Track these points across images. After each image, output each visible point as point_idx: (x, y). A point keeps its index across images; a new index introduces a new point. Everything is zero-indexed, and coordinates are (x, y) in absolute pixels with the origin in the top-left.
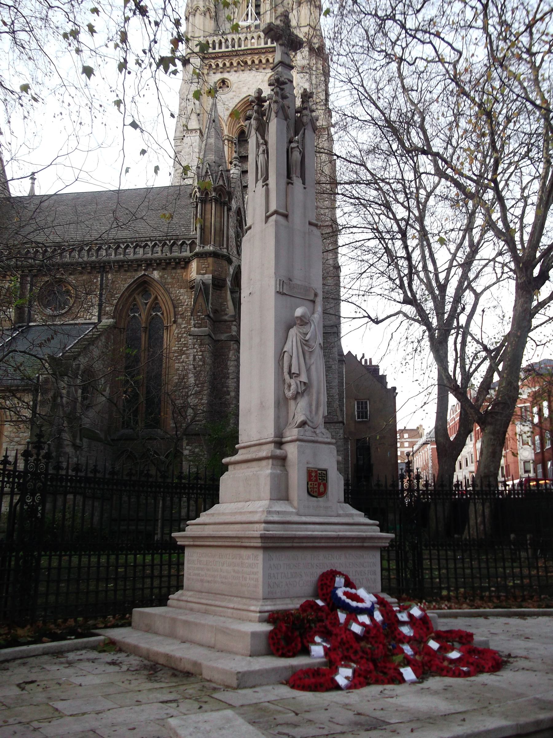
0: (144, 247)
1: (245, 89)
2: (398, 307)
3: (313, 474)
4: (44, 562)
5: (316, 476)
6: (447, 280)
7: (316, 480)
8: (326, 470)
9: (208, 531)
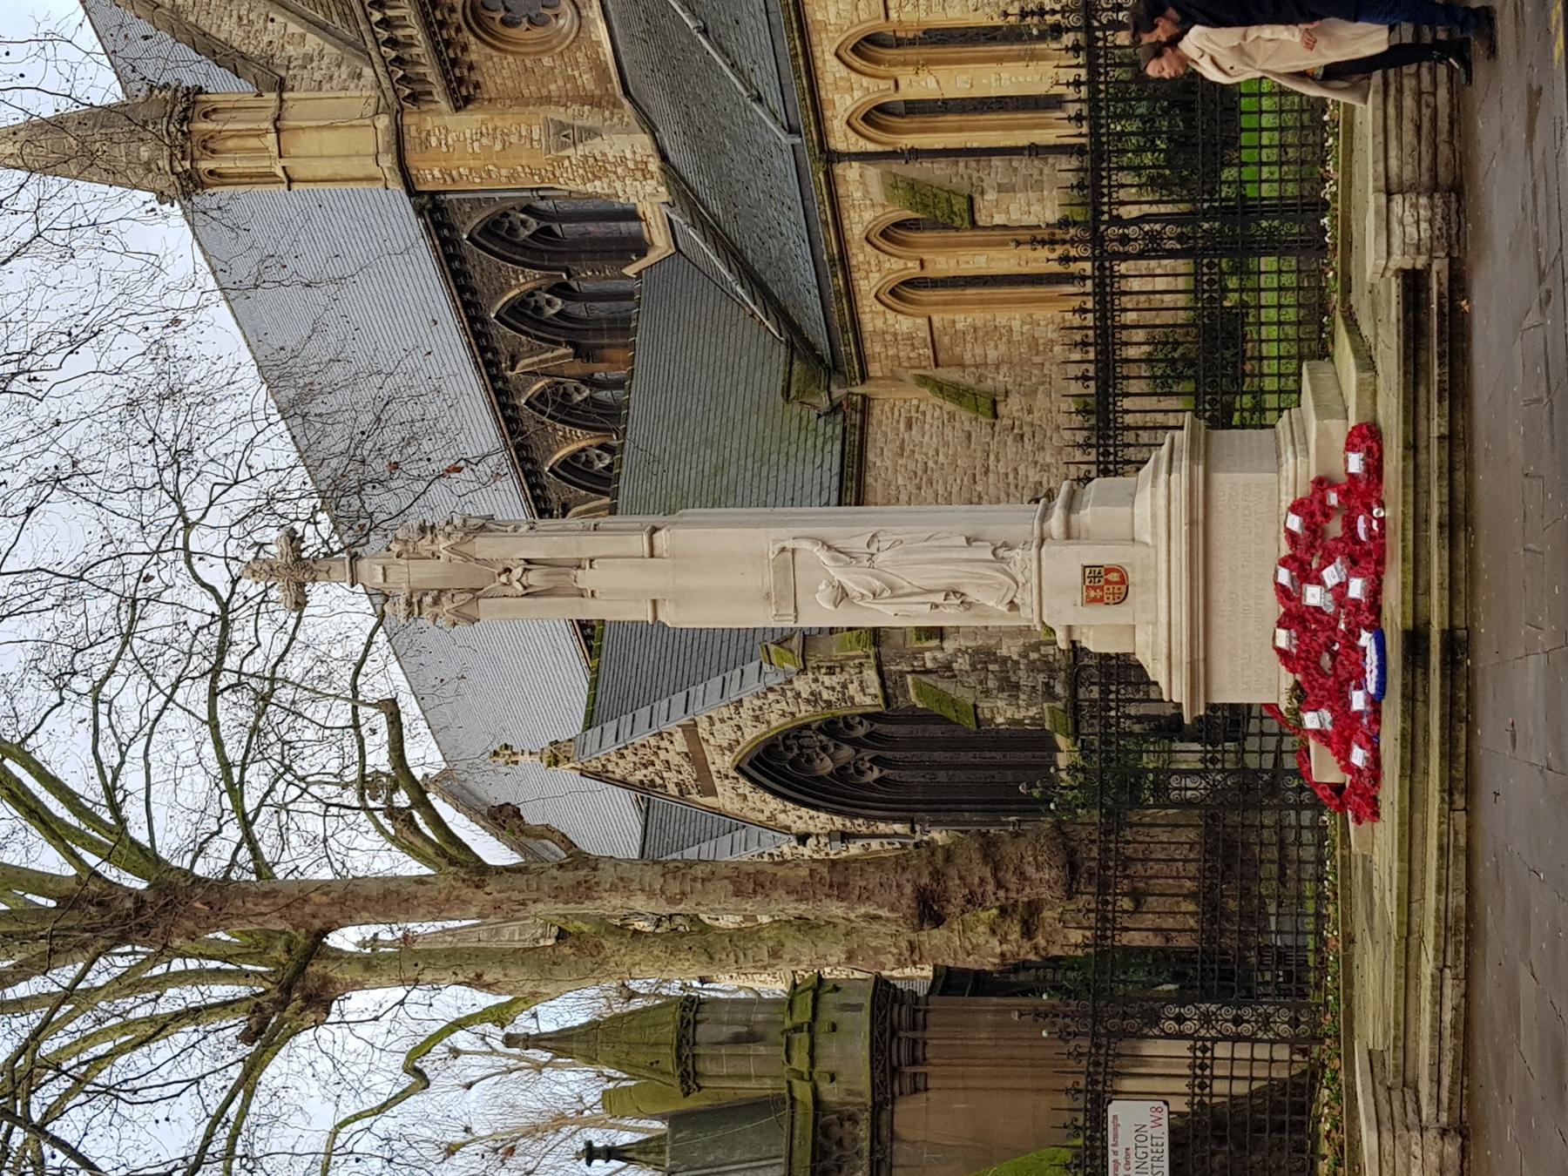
3: (1092, 594)
5: (1095, 589)
7: (1102, 589)
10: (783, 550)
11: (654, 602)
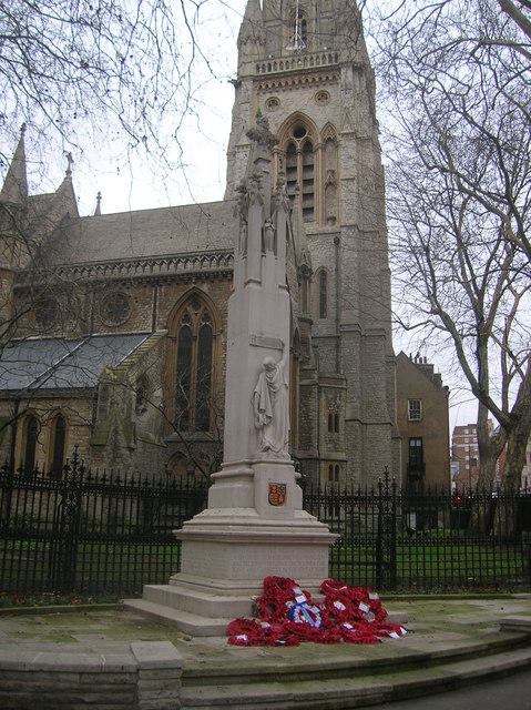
0: (194, 261)
1: (293, 106)
2: (427, 317)
4: (81, 547)
6: (485, 284)
8: (271, 489)
9: (195, 530)
10: (283, 345)
11: (260, 283)
